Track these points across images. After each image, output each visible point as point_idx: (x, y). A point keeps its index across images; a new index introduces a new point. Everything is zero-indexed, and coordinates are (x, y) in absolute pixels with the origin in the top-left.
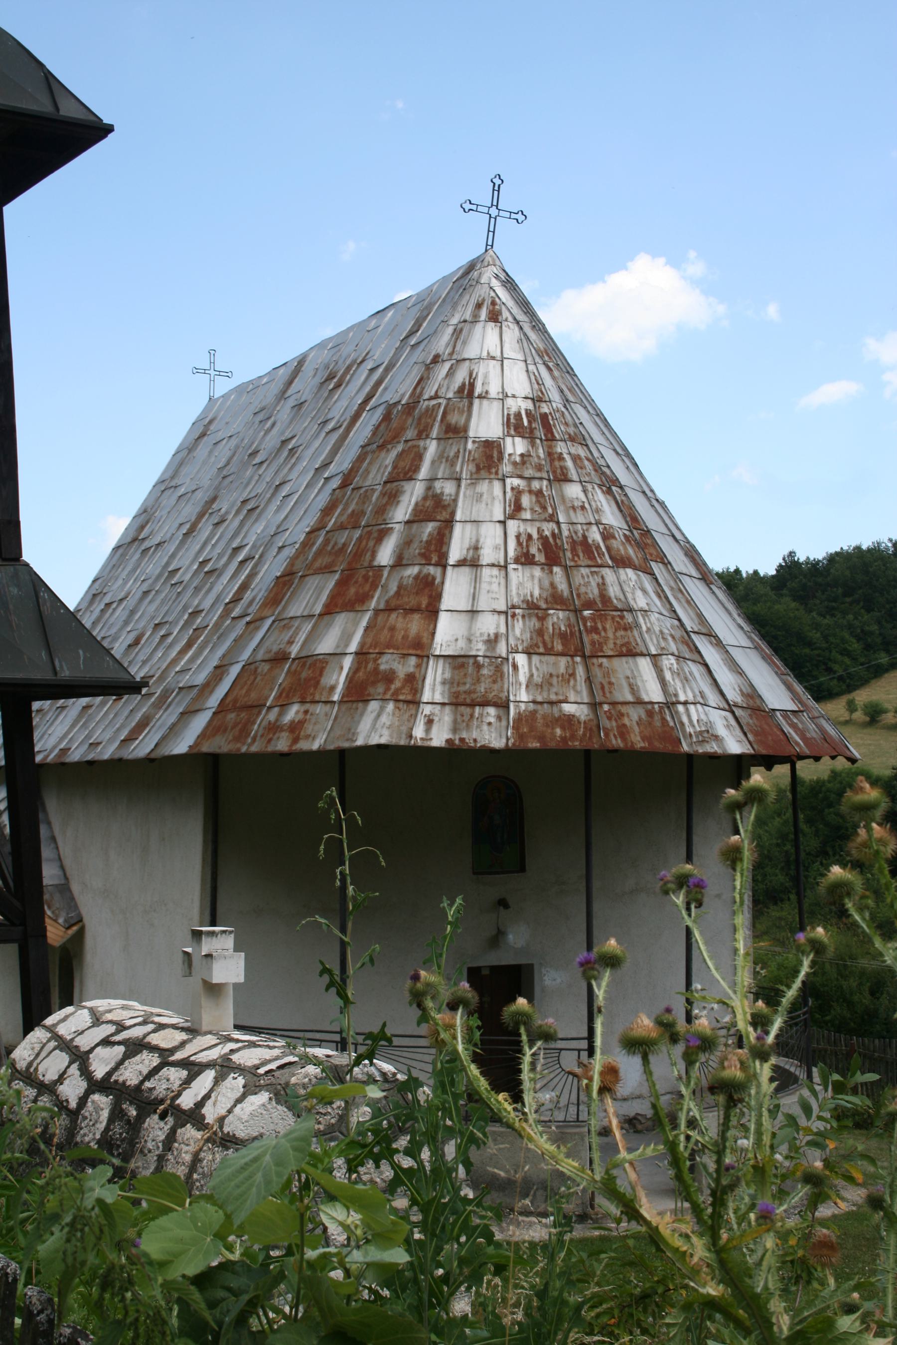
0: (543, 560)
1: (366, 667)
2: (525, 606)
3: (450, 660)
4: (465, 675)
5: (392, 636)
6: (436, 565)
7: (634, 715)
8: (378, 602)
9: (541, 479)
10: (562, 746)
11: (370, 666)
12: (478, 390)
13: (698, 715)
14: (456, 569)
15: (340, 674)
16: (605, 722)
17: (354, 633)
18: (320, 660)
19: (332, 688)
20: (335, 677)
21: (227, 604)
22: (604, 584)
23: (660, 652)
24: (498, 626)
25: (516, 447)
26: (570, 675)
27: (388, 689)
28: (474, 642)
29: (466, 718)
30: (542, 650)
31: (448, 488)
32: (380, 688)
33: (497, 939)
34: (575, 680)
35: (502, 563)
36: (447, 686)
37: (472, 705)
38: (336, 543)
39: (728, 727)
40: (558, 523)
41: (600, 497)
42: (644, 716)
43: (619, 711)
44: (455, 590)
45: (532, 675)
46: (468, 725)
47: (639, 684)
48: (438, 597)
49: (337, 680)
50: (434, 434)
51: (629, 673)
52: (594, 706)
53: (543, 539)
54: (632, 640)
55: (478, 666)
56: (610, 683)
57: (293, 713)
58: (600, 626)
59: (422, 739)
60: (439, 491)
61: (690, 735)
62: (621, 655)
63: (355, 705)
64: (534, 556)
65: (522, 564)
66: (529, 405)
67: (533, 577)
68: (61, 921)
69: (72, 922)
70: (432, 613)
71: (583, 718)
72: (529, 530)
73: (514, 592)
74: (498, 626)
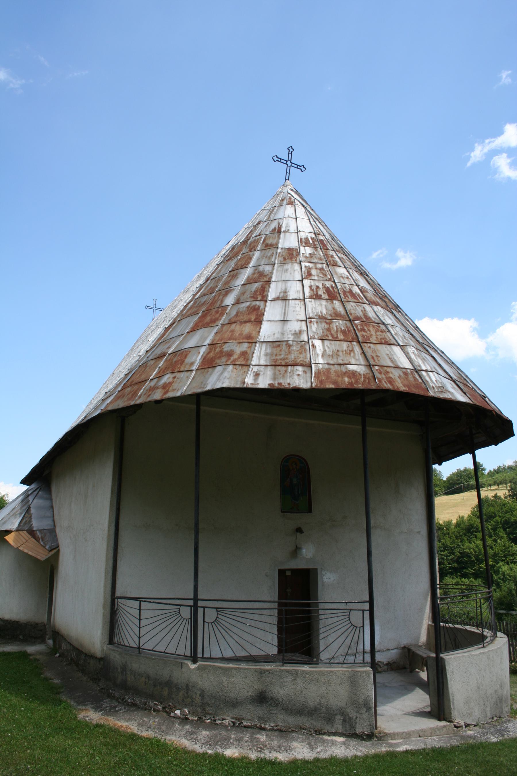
0: (327, 297)
1: (215, 351)
2: (317, 318)
3: (270, 344)
4: (281, 350)
5: (232, 335)
6: (260, 301)
7: (395, 374)
8: (224, 321)
9: (322, 263)
10: (350, 387)
11: (218, 350)
12: (283, 229)
13: (436, 378)
14: (273, 302)
15: (198, 356)
16: (377, 374)
17: (208, 336)
18: (186, 351)
19: (192, 364)
20: (194, 358)
22: (365, 311)
23: (405, 344)
24: (301, 326)
25: (306, 251)
26: (351, 351)
27: (229, 359)
28: (286, 334)
29: (282, 372)
30: (330, 338)
31: (268, 268)
32: (224, 359)
33: (296, 552)
34: (354, 353)
35: (302, 298)
36: (268, 357)
37: (287, 365)
38: (200, 302)
39: (453, 388)
40: (334, 282)
41: (356, 276)
42: (402, 374)
43: (386, 370)
44: (272, 312)
45: (325, 351)
46: (283, 376)
47: (395, 358)
48: (263, 314)
49: (196, 360)
50: (259, 248)
51: (388, 353)
52: (370, 366)
53: (327, 290)
54: (387, 337)
55: (289, 346)
56: (377, 356)
57: (167, 378)
58: (366, 328)
59: (251, 384)
60: (261, 270)
61: (433, 388)
62: (381, 343)
63: (206, 370)
64: (321, 295)
65: (314, 299)
66: (313, 236)
67: (321, 305)
68: (47, 547)
70: (259, 322)
71: (362, 373)
72: (317, 284)
73: (310, 311)
74: (301, 326)
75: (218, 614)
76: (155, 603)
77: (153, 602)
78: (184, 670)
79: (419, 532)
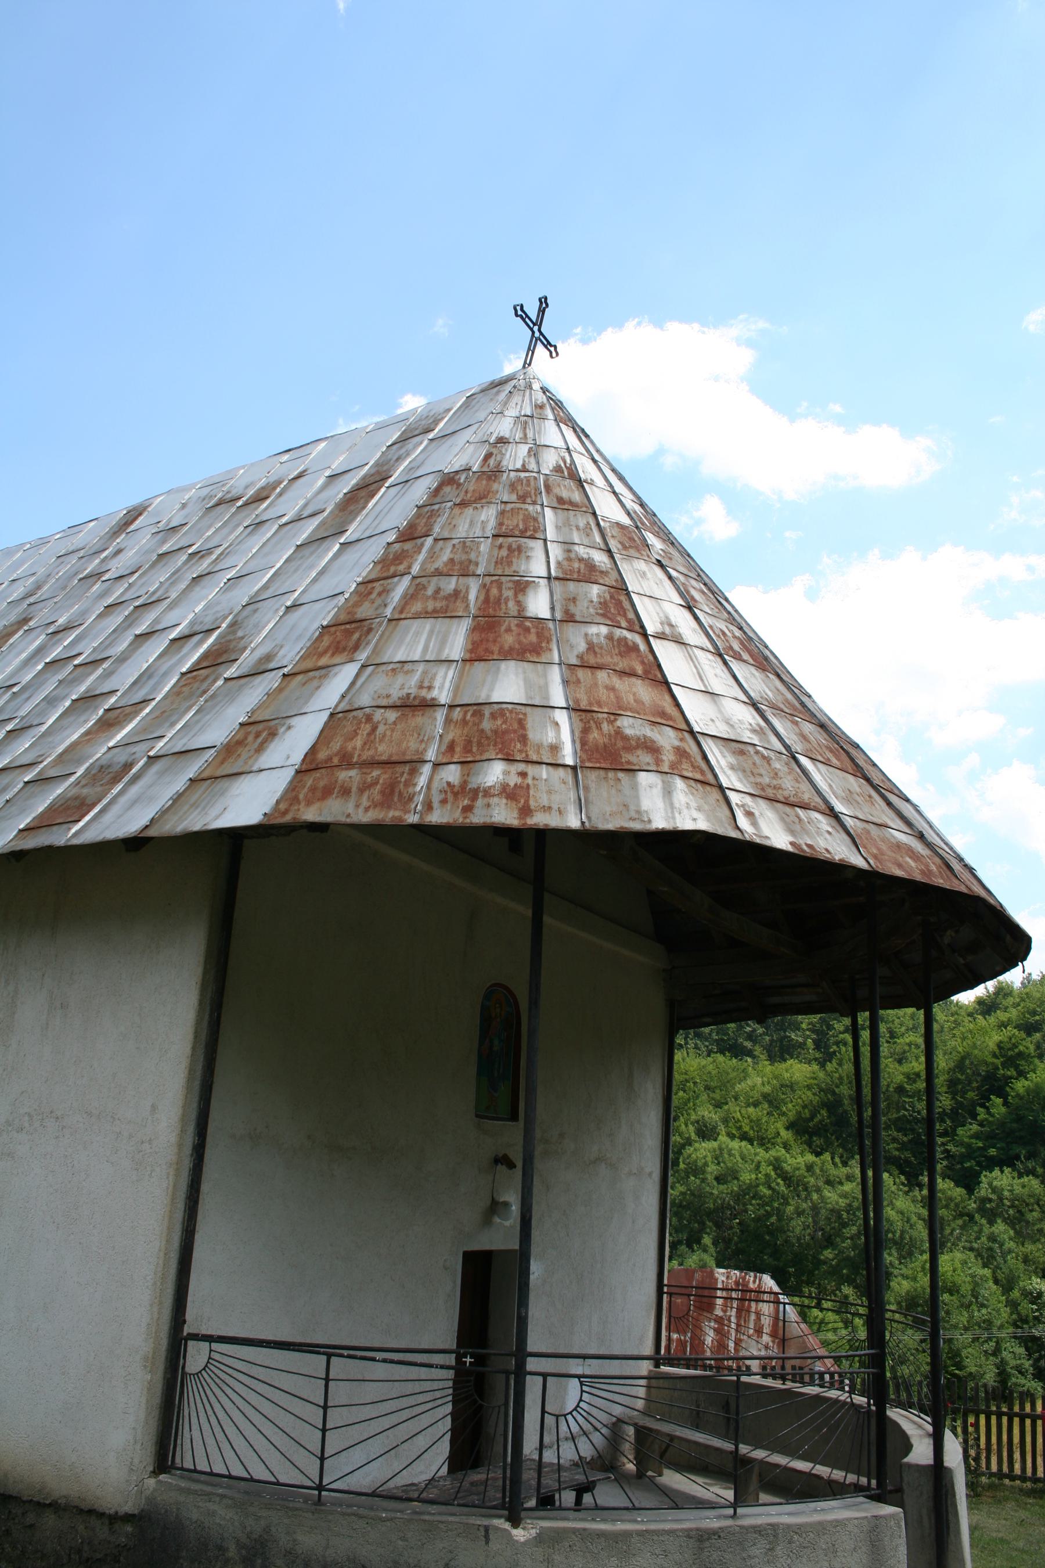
17: (546, 685)
21: (183, 674)
75: (582, 1391)
76: (392, 1362)
77: (385, 1361)
78: (494, 1545)
79: (650, 1174)
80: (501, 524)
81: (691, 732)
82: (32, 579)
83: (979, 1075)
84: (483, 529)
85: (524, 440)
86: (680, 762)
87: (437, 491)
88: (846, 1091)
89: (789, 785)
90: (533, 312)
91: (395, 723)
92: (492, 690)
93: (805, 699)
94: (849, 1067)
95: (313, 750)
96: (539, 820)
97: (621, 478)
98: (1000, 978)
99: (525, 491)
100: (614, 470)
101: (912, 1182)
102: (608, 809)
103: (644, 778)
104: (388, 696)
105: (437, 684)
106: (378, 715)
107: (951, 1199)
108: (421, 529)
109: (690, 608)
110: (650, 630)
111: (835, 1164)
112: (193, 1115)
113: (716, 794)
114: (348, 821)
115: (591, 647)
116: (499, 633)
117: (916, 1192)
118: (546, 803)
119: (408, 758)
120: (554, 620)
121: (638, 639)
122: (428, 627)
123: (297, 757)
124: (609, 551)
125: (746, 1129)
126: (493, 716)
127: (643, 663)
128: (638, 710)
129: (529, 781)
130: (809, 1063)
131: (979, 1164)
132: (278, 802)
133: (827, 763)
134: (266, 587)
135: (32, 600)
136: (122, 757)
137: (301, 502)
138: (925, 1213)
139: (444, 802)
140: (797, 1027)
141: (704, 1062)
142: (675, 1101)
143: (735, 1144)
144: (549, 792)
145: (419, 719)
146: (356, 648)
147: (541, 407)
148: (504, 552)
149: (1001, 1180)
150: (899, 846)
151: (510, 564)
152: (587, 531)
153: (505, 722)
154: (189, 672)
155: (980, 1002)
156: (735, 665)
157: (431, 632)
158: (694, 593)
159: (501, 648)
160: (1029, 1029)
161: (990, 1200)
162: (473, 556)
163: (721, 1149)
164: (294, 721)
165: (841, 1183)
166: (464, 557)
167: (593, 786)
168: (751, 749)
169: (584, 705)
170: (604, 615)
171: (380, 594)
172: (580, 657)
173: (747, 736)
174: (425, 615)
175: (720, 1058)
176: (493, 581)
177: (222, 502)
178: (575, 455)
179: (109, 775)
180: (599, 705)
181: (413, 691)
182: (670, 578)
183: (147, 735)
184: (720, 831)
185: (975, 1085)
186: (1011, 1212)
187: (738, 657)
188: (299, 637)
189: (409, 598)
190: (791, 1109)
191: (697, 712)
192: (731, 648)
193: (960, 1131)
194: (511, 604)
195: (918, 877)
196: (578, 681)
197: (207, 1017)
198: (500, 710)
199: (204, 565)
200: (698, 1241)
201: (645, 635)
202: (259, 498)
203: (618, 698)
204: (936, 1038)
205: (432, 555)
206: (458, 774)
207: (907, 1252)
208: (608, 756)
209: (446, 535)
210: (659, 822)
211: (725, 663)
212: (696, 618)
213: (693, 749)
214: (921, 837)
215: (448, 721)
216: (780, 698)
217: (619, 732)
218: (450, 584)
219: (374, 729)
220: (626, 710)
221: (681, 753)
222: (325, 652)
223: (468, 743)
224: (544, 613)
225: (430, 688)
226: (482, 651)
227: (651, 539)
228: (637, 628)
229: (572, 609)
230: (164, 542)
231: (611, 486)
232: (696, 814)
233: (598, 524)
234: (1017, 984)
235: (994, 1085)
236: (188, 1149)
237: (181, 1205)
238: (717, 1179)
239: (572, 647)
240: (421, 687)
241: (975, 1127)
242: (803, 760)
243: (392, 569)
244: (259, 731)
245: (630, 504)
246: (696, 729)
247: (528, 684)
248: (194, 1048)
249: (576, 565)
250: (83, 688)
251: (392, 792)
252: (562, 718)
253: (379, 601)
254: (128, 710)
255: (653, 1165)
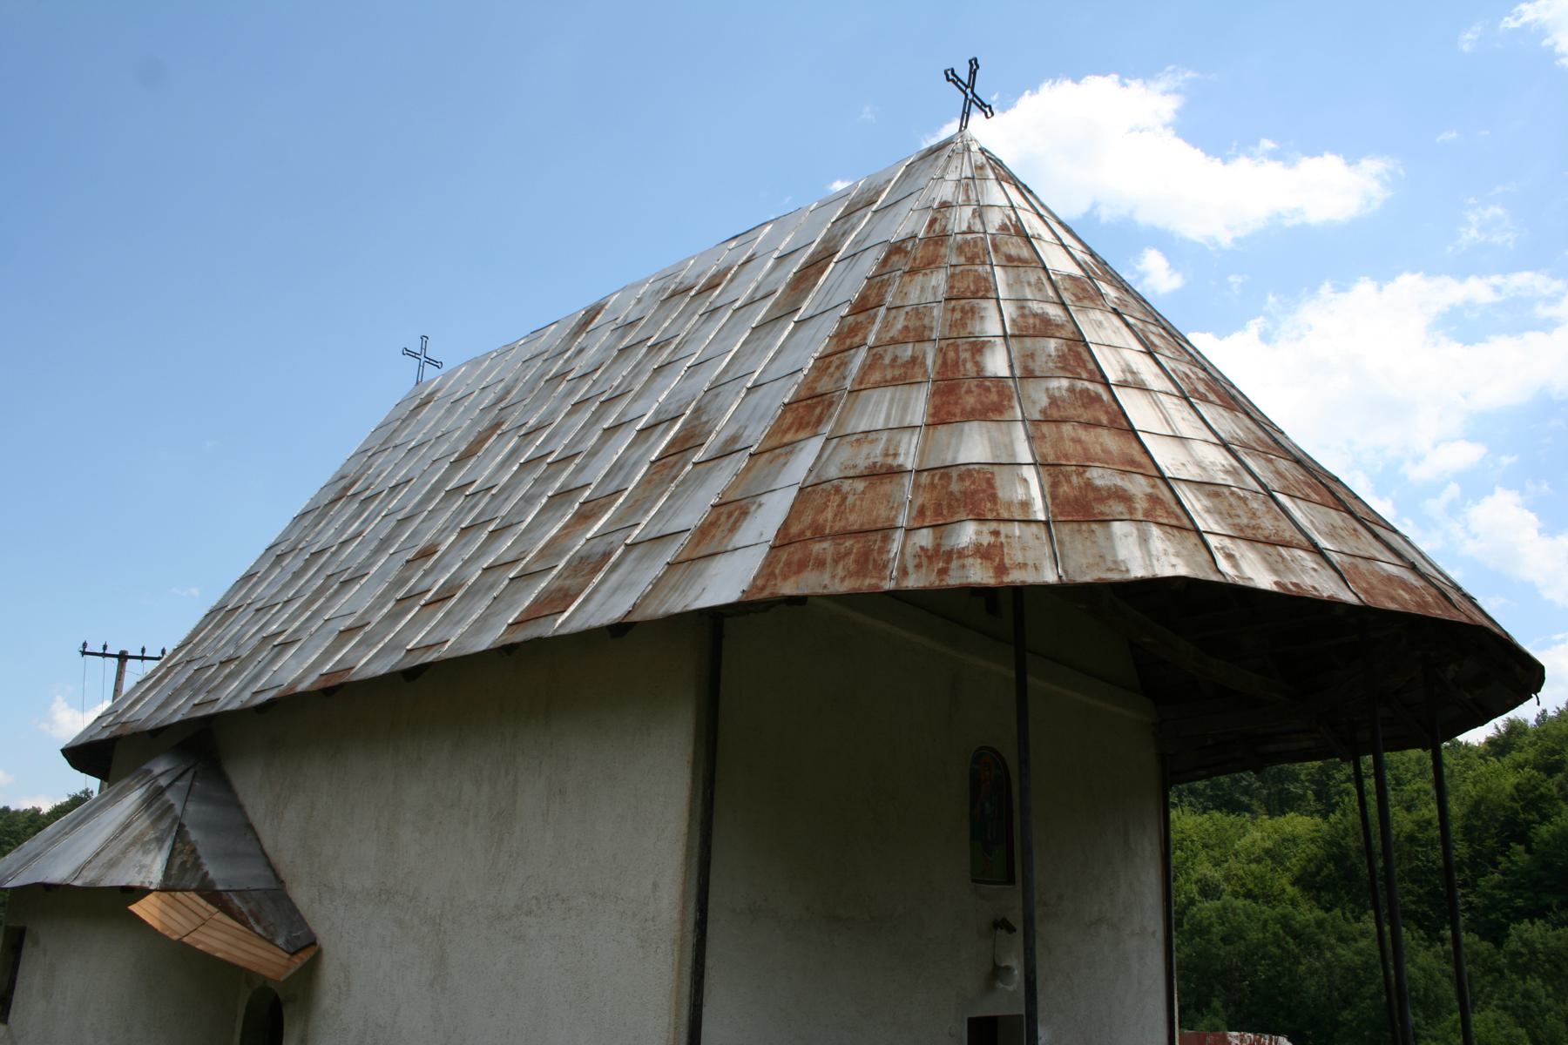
17: (1012, 443)
21: (652, 463)
68: (280, 941)
69: (300, 944)
79: (1154, 933)
80: (952, 287)
81: (1163, 478)
82: (501, 385)
83: (1497, 820)
84: (935, 294)
85: (967, 202)
86: (1154, 509)
87: (886, 260)
88: (1352, 843)
89: (1268, 524)
90: (964, 76)
91: (863, 492)
92: (957, 451)
93: (1277, 436)
94: (1354, 818)
95: (786, 525)
96: (1016, 577)
97: (1068, 230)
98: (1511, 714)
99: (973, 252)
100: (1060, 223)
101: (1433, 936)
102: (1084, 561)
103: (1117, 527)
104: (855, 467)
105: (902, 451)
106: (846, 486)
107: (1477, 954)
108: (873, 300)
109: (1150, 354)
110: (1112, 379)
111: (1346, 920)
112: (694, 892)
113: (1194, 539)
114: (826, 592)
115: (1053, 401)
116: (959, 396)
117: (1438, 946)
118: (1021, 560)
119: (879, 525)
120: (1013, 377)
121: (1100, 389)
122: (888, 395)
123: (770, 534)
124: (1063, 305)
125: (1251, 886)
126: (961, 478)
127: (1107, 412)
128: (1106, 460)
129: (1002, 539)
130: (1311, 814)
131: (1506, 916)
132: (755, 579)
133: (1306, 499)
134: (725, 371)
135: (502, 405)
136: (601, 547)
137: (753, 286)
138: (1450, 969)
139: (919, 566)
140: (1295, 778)
141: (1200, 820)
142: (1174, 862)
143: (1240, 903)
144: (1024, 549)
145: (887, 487)
146: (819, 422)
147: (982, 168)
148: (958, 315)
149: (1533, 931)
150: (1390, 579)
151: (964, 326)
152: (1039, 286)
153: (973, 483)
154: (658, 459)
155: (1491, 742)
156: (1201, 407)
157: (892, 399)
158: (1153, 338)
159: (963, 409)
160: (1551, 769)
161: (1522, 955)
162: (927, 321)
163: (1225, 908)
164: (764, 499)
165: (1355, 940)
166: (918, 323)
167: (1067, 539)
168: (1225, 490)
169: (1051, 459)
170: (1063, 368)
171: (838, 367)
172: (1043, 412)
173: (1221, 478)
174: (885, 383)
175: (1217, 815)
176: (948, 346)
177: (676, 294)
178: (1020, 212)
179: (588, 565)
180: (1066, 457)
181: (879, 459)
182: (1128, 325)
183: (623, 523)
184: (1201, 576)
185: (1493, 831)
186: (1547, 966)
187: (1204, 399)
188: (763, 417)
189: (867, 368)
190: (1294, 864)
191: (1166, 457)
192: (1196, 390)
193: (1481, 881)
194: (969, 365)
195: (1414, 610)
196: (1043, 436)
197: (700, 795)
198: (967, 471)
199: (664, 355)
200: (1208, 1005)
201: (1107, 384)
202: (711, 286)
203: (1085, 449)
204: (1447, 783)
205: (887, 324)
206: (931, 537)
207: (1433, 1010)
208: (1080, 508)
209: (898, 303)
210: (1138, 571)
211: (1192, 406)
212: (1158, 363)
213: (1165, 494)
214: (1413, 567)
215: (917, 486)
216: (1251, 436)
217: (1089, 484)
218: (907, 351)
219: (844, 499)
220: (1094, 460)
221: (1154, 500)
222: (789, 429)
223: (938, 506)
224: (1004, 371)
225: (895, 455)
226: (944, 415)
227: (1105, 288)
228: (1098, 378)
229: (1031, 365)
230: (623, 337)
231: (1059, 239)
232: (1174, 560)
233: (1049, 278)
234: (1532, 722)
235: (1515, 831)
236: (690, 925)
237: (687, 980)
238: (1223, 939)
239: (1034, 402)
240: (887, 455)
241: (1497, 877)
242: (1281, 498)
243: (848, 342)
244: (732, 511)
245: (1080, 255)
246: (1168, 474)
247: (994, 444)
248: (690, 826)
249: (1031, 321)
250: (558, 485)
251: (866, 560)
252: (1030, 474)
253: (837, 375)
254: (603, 501)
255: (1156, 924)
